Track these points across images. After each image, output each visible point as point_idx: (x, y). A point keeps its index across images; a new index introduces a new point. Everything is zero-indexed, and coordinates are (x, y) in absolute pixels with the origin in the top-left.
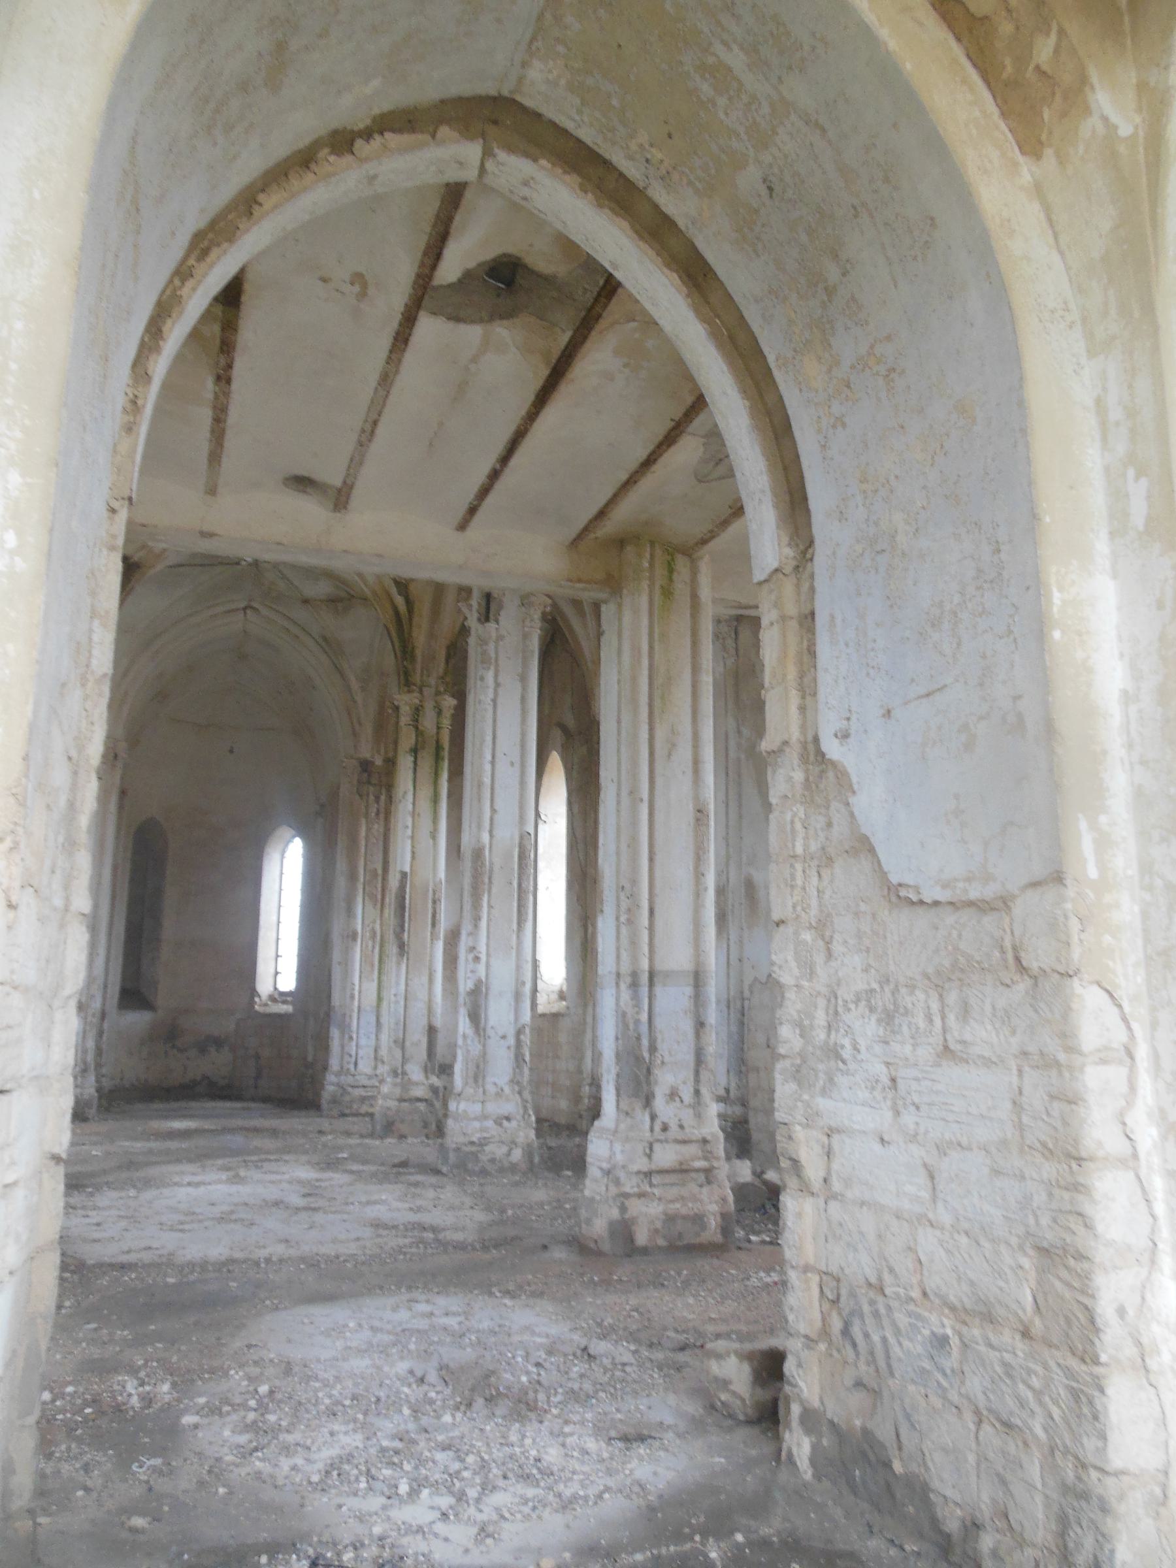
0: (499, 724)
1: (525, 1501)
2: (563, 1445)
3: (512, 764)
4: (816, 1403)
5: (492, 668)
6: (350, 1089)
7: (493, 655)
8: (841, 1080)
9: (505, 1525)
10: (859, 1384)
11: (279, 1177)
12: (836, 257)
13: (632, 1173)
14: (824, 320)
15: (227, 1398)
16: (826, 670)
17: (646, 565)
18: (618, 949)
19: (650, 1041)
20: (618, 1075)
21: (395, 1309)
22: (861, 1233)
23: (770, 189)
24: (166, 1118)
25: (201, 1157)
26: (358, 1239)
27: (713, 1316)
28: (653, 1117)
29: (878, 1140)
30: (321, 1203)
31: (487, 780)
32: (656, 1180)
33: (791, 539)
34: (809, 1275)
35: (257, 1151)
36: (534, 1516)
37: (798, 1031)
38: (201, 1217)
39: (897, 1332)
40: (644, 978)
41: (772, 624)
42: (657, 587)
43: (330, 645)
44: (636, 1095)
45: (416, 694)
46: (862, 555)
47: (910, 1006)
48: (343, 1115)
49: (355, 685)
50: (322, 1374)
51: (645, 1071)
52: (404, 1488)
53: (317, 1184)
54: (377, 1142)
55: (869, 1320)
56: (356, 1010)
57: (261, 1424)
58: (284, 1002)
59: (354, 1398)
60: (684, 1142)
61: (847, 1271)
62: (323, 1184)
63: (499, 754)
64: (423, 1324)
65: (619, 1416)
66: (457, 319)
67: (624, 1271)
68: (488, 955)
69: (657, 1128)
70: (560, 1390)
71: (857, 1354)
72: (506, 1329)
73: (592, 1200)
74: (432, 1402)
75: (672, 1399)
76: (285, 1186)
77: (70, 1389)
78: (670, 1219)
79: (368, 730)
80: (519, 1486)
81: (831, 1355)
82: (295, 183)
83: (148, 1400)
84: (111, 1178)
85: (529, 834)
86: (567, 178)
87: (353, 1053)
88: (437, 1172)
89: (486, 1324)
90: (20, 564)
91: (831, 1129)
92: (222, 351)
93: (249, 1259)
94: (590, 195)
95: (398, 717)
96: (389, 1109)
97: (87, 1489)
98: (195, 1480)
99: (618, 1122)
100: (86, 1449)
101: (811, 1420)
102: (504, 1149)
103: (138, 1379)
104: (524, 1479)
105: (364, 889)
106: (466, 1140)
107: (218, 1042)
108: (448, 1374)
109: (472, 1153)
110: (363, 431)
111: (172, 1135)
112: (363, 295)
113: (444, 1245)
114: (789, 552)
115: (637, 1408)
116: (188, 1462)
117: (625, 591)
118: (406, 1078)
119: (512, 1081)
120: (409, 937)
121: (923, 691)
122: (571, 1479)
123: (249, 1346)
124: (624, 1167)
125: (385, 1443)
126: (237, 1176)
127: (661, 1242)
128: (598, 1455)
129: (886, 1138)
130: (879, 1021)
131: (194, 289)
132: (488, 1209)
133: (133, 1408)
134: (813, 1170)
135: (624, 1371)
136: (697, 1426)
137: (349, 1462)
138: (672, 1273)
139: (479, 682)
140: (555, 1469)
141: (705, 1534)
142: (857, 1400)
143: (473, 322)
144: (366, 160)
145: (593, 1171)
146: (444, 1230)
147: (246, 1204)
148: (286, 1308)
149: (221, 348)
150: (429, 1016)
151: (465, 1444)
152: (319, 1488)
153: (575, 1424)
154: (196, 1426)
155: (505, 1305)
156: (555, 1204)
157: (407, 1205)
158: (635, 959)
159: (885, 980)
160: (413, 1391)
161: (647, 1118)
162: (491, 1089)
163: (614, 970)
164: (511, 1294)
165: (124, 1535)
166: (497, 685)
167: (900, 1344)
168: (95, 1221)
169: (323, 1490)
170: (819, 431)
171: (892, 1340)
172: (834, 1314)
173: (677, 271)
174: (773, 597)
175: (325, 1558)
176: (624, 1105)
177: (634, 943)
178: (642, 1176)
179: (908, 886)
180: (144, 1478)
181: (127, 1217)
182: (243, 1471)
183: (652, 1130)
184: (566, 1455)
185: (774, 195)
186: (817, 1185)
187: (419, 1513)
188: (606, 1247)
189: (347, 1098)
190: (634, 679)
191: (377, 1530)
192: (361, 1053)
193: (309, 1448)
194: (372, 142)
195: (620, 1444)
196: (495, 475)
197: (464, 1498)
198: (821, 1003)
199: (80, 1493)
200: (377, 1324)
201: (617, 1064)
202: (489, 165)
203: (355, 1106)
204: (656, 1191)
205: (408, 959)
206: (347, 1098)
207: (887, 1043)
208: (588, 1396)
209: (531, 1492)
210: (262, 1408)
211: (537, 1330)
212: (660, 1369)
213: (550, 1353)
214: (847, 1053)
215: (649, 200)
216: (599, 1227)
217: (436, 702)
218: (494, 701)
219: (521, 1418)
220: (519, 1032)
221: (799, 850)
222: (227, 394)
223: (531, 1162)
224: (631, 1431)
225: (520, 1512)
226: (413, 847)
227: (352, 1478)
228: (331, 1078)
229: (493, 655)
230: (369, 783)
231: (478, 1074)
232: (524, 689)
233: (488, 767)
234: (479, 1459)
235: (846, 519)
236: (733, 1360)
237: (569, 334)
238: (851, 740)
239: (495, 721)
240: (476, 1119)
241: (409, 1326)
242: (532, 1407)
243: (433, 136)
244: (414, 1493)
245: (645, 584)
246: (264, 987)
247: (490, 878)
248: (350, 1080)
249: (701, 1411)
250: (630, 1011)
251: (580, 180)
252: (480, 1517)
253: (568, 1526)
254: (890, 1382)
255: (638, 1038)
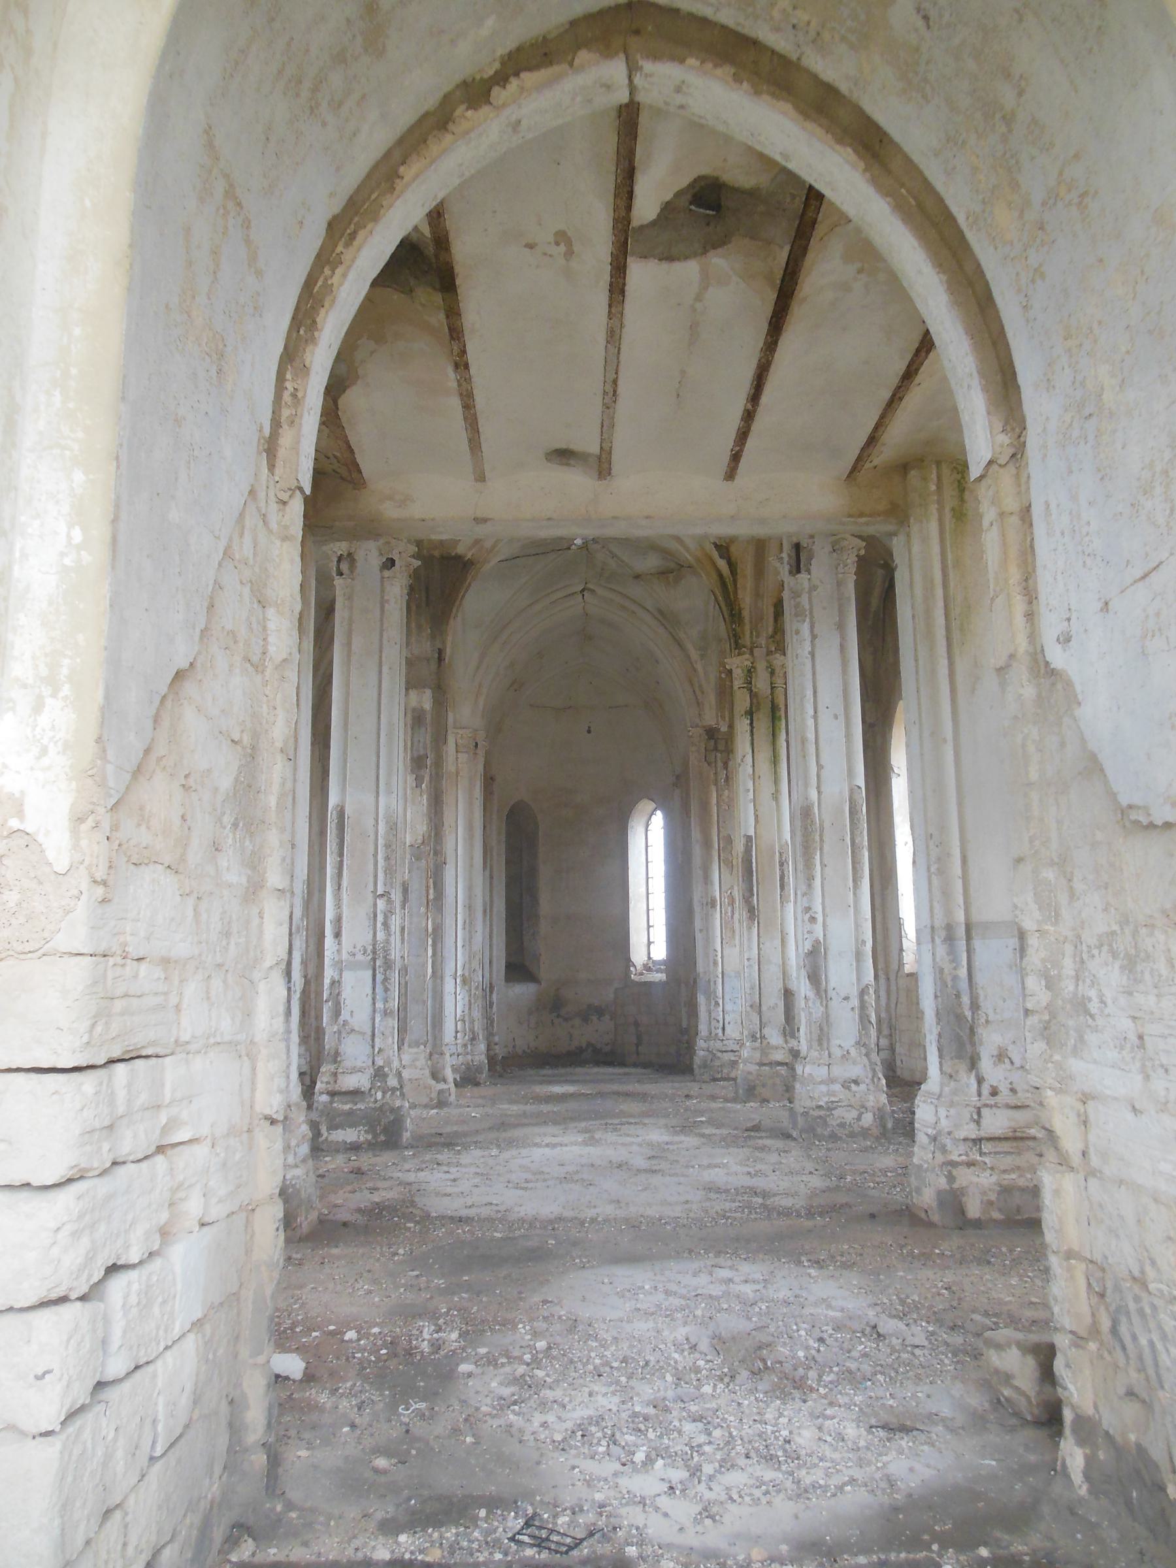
0: (818, 676)
1: (761, 1483)
2: (820, 1428)
3: (836, 717)
4: (1090, 1411)
5: (808, 620)
6: (719, 1054)
7: (807, 607)
8: (1091, 1038)
9: (731, 1506)
10: (1131, 1394)
11: (629, 1139)
12: (1008, 76)
13: (959, 1140)
14: (1008, 156)
15: (507, 1350)
16: (1045, 567)
17: (933, 488)
18: (931, 901)
19: (971, 997)
20: (940, 1035)
21: (695, 1274)
22: (1121, 1217)
23: (926, 18)
24: (550, 1083)
25: (561, 1121)
26: (687, 1202)
27: (1034, 1300)
28: (980, 1081)
29: (1130, 1109)
30: (664, 1165)
31: (811, 736)
32: (987, 1147)
33: (1006, 423)
34: (1073, 1261)
35: (622, 1114)
36: (764, 1500)
37: (1043, 983)
38: (547, 1176)
39: (1164, 1337)
40: (961, 932)
41: (992, 524)
42: (947, 510)
43: (665, 618)
44: (959, 1056)
45: (747, 656)
46: (1071, 425)
47: (1150, 949)
48: (715, 1080)
49: (694, 654)
50: (603, 1334)
51: (967, 1031)
52: (640, 1457)
53: (666, 1147)
54: (739, 1106)
55: (1136, 1319)
56: (720, 976)
57: (528, 1379)
58: (657, 971)
59: (624, 1360)
60: (1017, 1107)
61: (1110, 1261)
62: (671, 1147)
63: (820, 707)
64: (716, 1290)
65: (891, 1402)
66: (670, 258)
67: (950, 1245)
68: (825, 915)
69: (986, 1091)
70: (835, 1369)
71: (1127, 1357)
72: (802, 1300)
73: (920, 1167)
74: (697, 1370)
75: (958, 1389)
76: (635, 1148)
77: (376, 1330)
78: (1006, 1190)
79: (711, 698)
80: (758, 1467)
81: (1102, 1357)
82: (434, 148)
83: (436, 1346)
84: (480, 1138)
85: (859, 788)
86: (719, 71)
87: (720, 1018)
88: (788, 1136)
89: (783, 1294)
90: (86, 557)
91: (1084, 1094)
92: (452, 338)
93: (576, 1218)
94: (745, 84)
95: (732, 681)
96: (750, 1073)
97: (353, 1426)
98: (450, 1427)
99: (942, 1085)
100: (368, 1388)
101: (1087, 1430)
102: (854, 1114)
103: (436, 1325)
104: (767, 1461)
105: (719, 856)
106: (814, 1104)
107: (600, 1011)
108: (720, 1343)
109: (820, 1117)
110: (605, 393)
111: (550, 1099)
112: (569, 253)
113: (768, 1210)
114: (1004, 439)
115: (914, 1396)
116: (451, 1409)
117: (912, 520)
118: (765, 1042)
119: (858, 1043)
120: (758, 901)
121: (1139, 573)
122: (816, 1465)
123: (545, 1302)
124: (949, 1133)
125: (637, 1409)
126: (593, 1137)
127: (996, 1215)
128: (855, 1443)
129: (1137, 1107)
130: (1122, 968)
131: (344, 275)
132: (827, 1175)
133: (422, 1352)
134: (1071, 1143)
135: (913, 1354)
136: (978, 1422)
137: (597, 1424)
138: (1004, 1249)
139: (795, 636)
140: (803, 1452)
141: (944, 1547)
142: (1131, 1410)
143: (686, 258)
144: (504, 105)
145: (921, 1138)
146: (775, 1195)
147: (592, 1165)
148: (593, 1267)
149: (451, 336)
150: (784, 980)
151: (718, 1418)
152: (561, 1447)
153: (840, 1406)
154: (470, 1375)
155: (809, 1275)
156: (900, 1171)
157: (746, 1169)
158: (948, 912)
159: (1124, 921)
160: (684, 1357)
161: (973, 1081)
162: (838, 1053)
163: (929, 926)
164: (818, 1264)
165: (368, 1474)
166: (814, 637)
167: (1167, 1350)
168: (452, 1177)
169: (563, 1450)
170: (1019, 291)
171: (1159, 1346)
172: (1102, 1308)
173: (851, 145)
174: (990, 493)
175: (541, 1520)
176: (948, 1069)
177: (946, 894)
178: (971, 1144)
179: (1138, 808)
180: (406, 1420)
181: (482, 1174)
182: (495, 1423)
183: (979, 1095)
184: (820, 1439)
185: (931, 24)
186: (1076, 1160)
187: (647, 1484)
188: (935, 1218)
189: (717, 1063)
190: (928, 612)
191: (599, 1497)
192: (727, 1019)
193: (564, 1407)
194: (508, 86)
195: (882, 1433)
196: (749, 416)
197: (698, 1474)
198: (1069, 949)
199: (346, 1429)
200: (673, 1287)
201: (938, 1024)
202: (638, 80)
203: (725, 1071)
204: (987, 1160)
205: (758, 923)
206: (717, 1063)
207: (1130, 994)
208: (865, 1379)
209: (769, 1475)
210: (536, 1362)
211: (834, 1303)
212: (955, 1354)
213: (837, 1329)
214: (1094, 1007)
215: (807, 71)
216: (927, 1198)
217: (768, 661)
218: (812, 654)
219: (785, 1396)
220: (863, 993)
221: (1034, 775)
222: (469, 380)
223: (884, 1127)
224: (894, 1421)
225: (751, 1495)
226: (756, 810)
227: (595, 1441)
228: (701, 1043)
229: (807, 607)
230: (716, 749)
231: (822, 1037)
232: (843, 638)
233: (810, 722)
234: (727, 1434)
235: (1054, 387)
236: (1014, 1352)
237: (787, 248)
238: (1073, 643)
239: (814, 674)
240: (821, 1082)
241: (704, 1291)
242: (800, 1384)
243: (571, 64)
244: (649, 1461)
245: (933, 508)
246: (638, 956)
247: (821, 836)
248: (719, 1045)
249: (987, 1405)
250: (947, 968)
251: (733, 71)
252: (708, 1495)
253: (797, 1517)
254: (1161, 1393)
255: (958, 996)
